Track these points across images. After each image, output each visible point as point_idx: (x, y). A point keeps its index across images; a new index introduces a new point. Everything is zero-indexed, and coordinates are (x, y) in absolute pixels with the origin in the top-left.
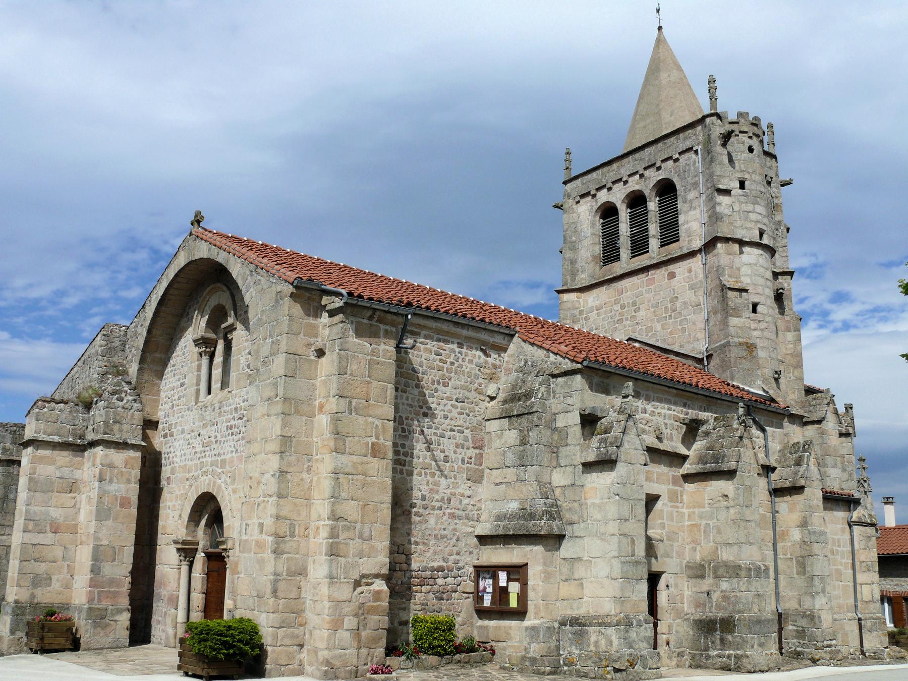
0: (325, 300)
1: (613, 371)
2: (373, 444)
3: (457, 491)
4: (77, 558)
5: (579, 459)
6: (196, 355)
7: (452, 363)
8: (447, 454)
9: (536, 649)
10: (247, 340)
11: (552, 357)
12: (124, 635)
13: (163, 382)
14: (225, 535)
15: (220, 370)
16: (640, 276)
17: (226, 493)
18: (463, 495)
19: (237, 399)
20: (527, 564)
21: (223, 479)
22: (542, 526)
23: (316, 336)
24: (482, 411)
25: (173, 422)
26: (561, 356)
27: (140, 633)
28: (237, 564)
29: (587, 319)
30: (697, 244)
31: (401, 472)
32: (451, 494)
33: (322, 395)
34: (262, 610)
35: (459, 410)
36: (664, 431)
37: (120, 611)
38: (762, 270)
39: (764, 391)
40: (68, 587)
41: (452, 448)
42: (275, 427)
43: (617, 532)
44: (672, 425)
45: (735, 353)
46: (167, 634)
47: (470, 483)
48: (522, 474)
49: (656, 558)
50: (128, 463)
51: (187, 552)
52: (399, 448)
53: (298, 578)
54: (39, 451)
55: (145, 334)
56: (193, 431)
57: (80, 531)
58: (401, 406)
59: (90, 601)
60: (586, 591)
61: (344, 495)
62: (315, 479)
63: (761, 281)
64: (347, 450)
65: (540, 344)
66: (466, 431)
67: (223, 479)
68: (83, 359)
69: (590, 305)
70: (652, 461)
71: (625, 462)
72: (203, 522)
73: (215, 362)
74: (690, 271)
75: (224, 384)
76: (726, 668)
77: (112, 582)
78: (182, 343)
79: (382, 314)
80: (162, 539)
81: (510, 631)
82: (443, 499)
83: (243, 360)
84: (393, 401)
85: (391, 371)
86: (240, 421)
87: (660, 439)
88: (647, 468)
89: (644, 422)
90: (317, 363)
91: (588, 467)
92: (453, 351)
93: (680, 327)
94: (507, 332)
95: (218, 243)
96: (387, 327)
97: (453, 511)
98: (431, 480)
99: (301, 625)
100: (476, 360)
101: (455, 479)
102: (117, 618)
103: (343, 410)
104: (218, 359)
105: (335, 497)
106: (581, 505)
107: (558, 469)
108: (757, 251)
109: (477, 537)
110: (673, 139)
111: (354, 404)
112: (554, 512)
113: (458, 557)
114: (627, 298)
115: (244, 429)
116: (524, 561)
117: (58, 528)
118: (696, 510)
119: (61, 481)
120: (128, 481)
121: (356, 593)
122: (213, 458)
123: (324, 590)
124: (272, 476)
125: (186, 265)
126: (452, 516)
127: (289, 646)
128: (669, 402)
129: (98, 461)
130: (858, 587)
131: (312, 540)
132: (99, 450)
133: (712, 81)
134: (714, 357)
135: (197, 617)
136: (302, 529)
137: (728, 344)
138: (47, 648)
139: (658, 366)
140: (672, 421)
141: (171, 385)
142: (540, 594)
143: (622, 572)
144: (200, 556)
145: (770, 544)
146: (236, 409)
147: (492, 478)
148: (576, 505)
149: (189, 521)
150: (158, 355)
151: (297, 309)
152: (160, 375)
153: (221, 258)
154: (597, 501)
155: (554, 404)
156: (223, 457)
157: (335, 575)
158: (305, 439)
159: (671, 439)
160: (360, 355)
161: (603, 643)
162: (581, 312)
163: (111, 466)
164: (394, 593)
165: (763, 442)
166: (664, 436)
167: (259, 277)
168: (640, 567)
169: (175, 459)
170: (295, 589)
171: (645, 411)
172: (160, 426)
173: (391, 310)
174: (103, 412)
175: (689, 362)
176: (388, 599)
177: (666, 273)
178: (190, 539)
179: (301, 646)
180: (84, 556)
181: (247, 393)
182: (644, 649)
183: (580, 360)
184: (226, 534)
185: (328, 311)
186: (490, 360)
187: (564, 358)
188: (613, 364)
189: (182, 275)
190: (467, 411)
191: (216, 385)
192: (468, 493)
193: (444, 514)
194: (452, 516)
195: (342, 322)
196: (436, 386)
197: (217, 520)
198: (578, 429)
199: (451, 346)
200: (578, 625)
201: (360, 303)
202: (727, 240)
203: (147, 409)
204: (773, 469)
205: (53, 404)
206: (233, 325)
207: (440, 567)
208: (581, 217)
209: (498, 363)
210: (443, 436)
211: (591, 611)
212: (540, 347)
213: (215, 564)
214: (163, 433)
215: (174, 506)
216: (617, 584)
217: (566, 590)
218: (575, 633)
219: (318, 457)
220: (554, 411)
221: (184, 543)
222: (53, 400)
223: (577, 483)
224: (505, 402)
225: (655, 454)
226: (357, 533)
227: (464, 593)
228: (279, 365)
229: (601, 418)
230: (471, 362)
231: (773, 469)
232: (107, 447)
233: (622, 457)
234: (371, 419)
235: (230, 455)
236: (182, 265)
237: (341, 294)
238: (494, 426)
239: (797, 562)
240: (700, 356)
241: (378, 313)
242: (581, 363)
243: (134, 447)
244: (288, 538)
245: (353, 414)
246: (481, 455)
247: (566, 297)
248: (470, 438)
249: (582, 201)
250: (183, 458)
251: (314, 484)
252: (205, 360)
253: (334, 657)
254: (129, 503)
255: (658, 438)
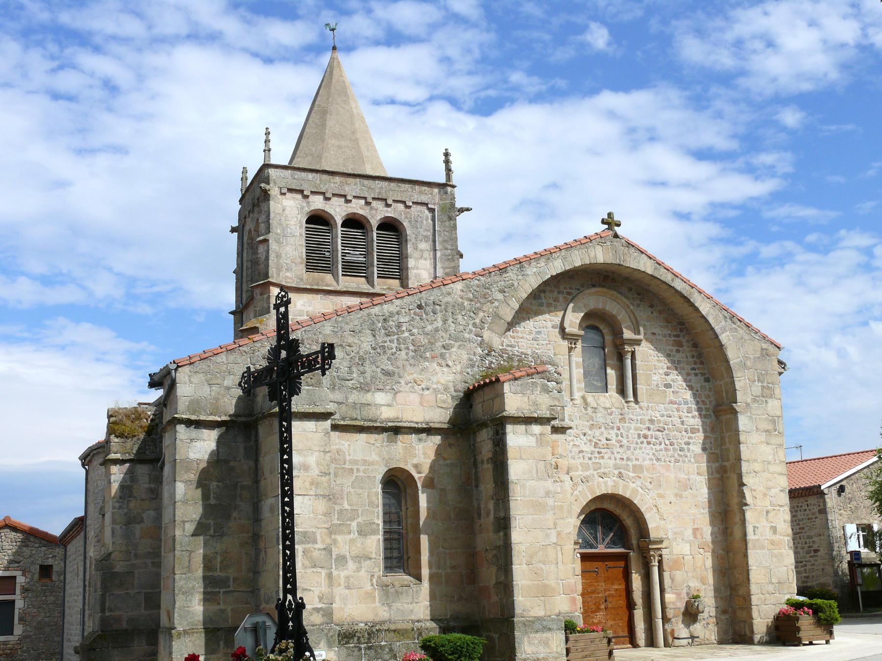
110: (407, 186)
133: (447, 154)
206: (641, 340)
208: (287, 212)
249: (289, 195)
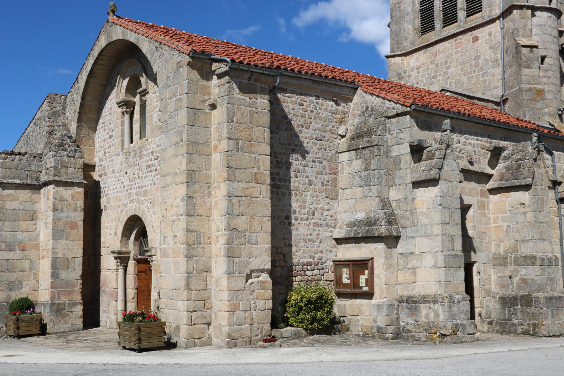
0: (215, 66)
1: (434, 112)
2: (255, 174)
3: (319, 206)
4: (41, 268)
5: (410, 178)
6: (120, 114)
7: (312, 111)
8: (310, 179)
9: (382, 322)
10: (157, 101)
11: (387, 103)
12: (79, 322)
13: (97, 135)
14: (150, 245)
15: (138, 124)
16: (451, 41)
17: (148, 215)
18: (323, 209)
19: (152, 145)
20: (373, 258)
21: (145, 205)
22: (382, 229)
23: (209, 94)
24: (335, 146)
25: (106, 165)
26: (394, 102)
27: (91, 319)
28: (159, 266)
29: (409, 76)
30: (497, 12)
31: (277, 193)
32: (314, 208)
33: (216, 138)
34: (179, 299)
35: (318, 146)
36: (474, 156)
37: (74, 305)
38: (550, 29)
39: (550, 124)
40: (36, 289)
41: (314, 174)
42: (181, 164)
43: (440, 233)
44: (480, 152)
45: (525, 97)
46: (110, 320)
47: (328, 200)
48: (367, 192)
49: (475, 252)
50: (75, 196)
51: (122, 259)
52: (275, 176)
53: (205, 275)
54: (5, 191)
55: (80, 100)
56: (121, 171)
57: (41, 248)
58: (275, 145)
59: (52, 298)
60: (419, 278)
61: (236, 212)
62: (213, 201)
63: (549, 38)
64: (237, 178)
65: (377, 94)
66: (324, 161)
67: (145, 205)
68: (34, 121)
69: (411, 66)
70: (466, 179)
71: (445, 180)
72: (133, 237)
73: (134, 119)
74: (490, 34)
75: (143, 134)
76: (526, 333)
77: (68, 284)
78: (108, 105)
80: (103, 251)
81: (361, 308)
82: (308, 212)
83: (155, 116)
84: (269, 141)
85: (266, 119)
86: (156, 161)
87: (471, 163)
88: (461, 185)
89: (458, 150)
90: (211, 114)
91: (417, 184)
92: (312, 102)
93: (482, 79)
94: (352, 86)
95: (130, 27)
96: (263, 85)
97: (316, 221)
98: (300, 199)
99: (208, 309)
100: (329, 108)
101: (317, 197)
102: (73, 310)
103: (232, 149)
104: (137, 116)
105: (230, 214)
106: (412, 213)
107: (394, 187)
108: (545, 14)
109: (335, 239)
111: (240, 144)
112: (391, 220)
113: (321, 255)
114: (441, 58)
115: (159, 167)
116: (372, 257)
117: (24, 246)
118: (500, 216)
119: (24, 212)
120: (75, 210)
121: (248, 283)
122: (137, 190)
123: (224, 282)
124: (182, 200)
125: (107, 46)
126: (316, 225)
127: (200, 324)
128: (476, 134)
129: (51, 197)
131: (213, 246)
132: (51, 188)
134: (509, 100)
135: (132, 307)
136: (206, 238)
137: (521, 90)
138: (21, 334)
139: (467, 108)
140: (480, 149)
141: (103, 138)
142: (384, 280)
143: (445, 262)
144: (132, 264)
145: (558, 240)
146: (152, 152)
147: (345, 196)
148: (408, 213)
149: (122, 237)
150: (90, 116)
151: (195, 74)
152: (95, 130)
153: (132, 37)
154: (425, 210)
155: (390, 139)
156: (144, 189)
157: (232, 271)
158: (205, 172)
159: (479, 162)
161: (432, 315)
162: (405, 71)
163: (62, 199)
164: (276, 283)
165: (551, 163)
166: (474, 161)
167: (163, 52)
168: (458, 259)
169: (109, 192)
170: (203, 282)
171: (459, 142)
172: (97, 169)
173: (265, 72)
174: (52, 160)
175: (490, 105)
176: (271, 287)
177: (471, 38)
178: (124, 249)
179: (209, 324)
180: (45, 266)
181: (160, 140)
182: (463, 319)
183: (409, 105)
184: (150, 245)
185: (217, 75)
186: (340, 108)
187: (396, 103)
188: (434, 107)
189: (104, 53)
190: (324, 147)
191: (136, 136)
192: (327, 207)
193: (310, 223)
194: (316, 225)
195: (228, 82)
196: (300, 128)
197: (143, 234)
198: (409, 157)
199: (310, 98)
200: (412, 303)
201: (241, 67)
202: (521, 7)
203: (86, 156)
204: (560, 183)
205: (13, 156)
207: (308, 262)
209: (346, 110)
210: (307, 166)
211: (422, 292)
212: (378, 96)
213: (143, 266)
214: (99, 173)
215: (111, 226)
216: (442, 271)
217: (402, 276)
218: (409, 308)
219: (216, 184)
220: (389, 144)
221: (119, 252)
222: (12, 153)
223: (408, 197)
224: (353, 138)
225: (469, 175)
226: (247, 239)
227: (326, 281)
228: (182, 117)
229: (426, 148)
230: (326, 110)
231: (560, 183)
232: (57, 186)
233: (443, 177)
234: (253, 155)
235: (149, 187)
236: (104, 45)
237: (226, 61)
238: (344, 157)
240: (498, 100)
241: (254, 75)
242: (410, 107)
243: (78, 185)
244: (196, 246)
245: (240, 152)
246: (336, 179)
247: (393, 60)
248: (327, 166)
250: (115, 191)
251: (213, 204)
252: (127, 117)
253: (235, 331)
254: (77, 226)
255: (469, 162)
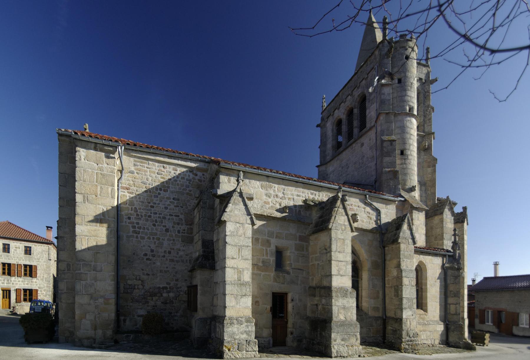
8: (167, 227)
79: (101, 146)
126: (172, 260)
130: (448, 306)
160: (90, 170)
193: (167, 259)
196: (159, 191)
210: (164, 218)
239: (395, 289)
